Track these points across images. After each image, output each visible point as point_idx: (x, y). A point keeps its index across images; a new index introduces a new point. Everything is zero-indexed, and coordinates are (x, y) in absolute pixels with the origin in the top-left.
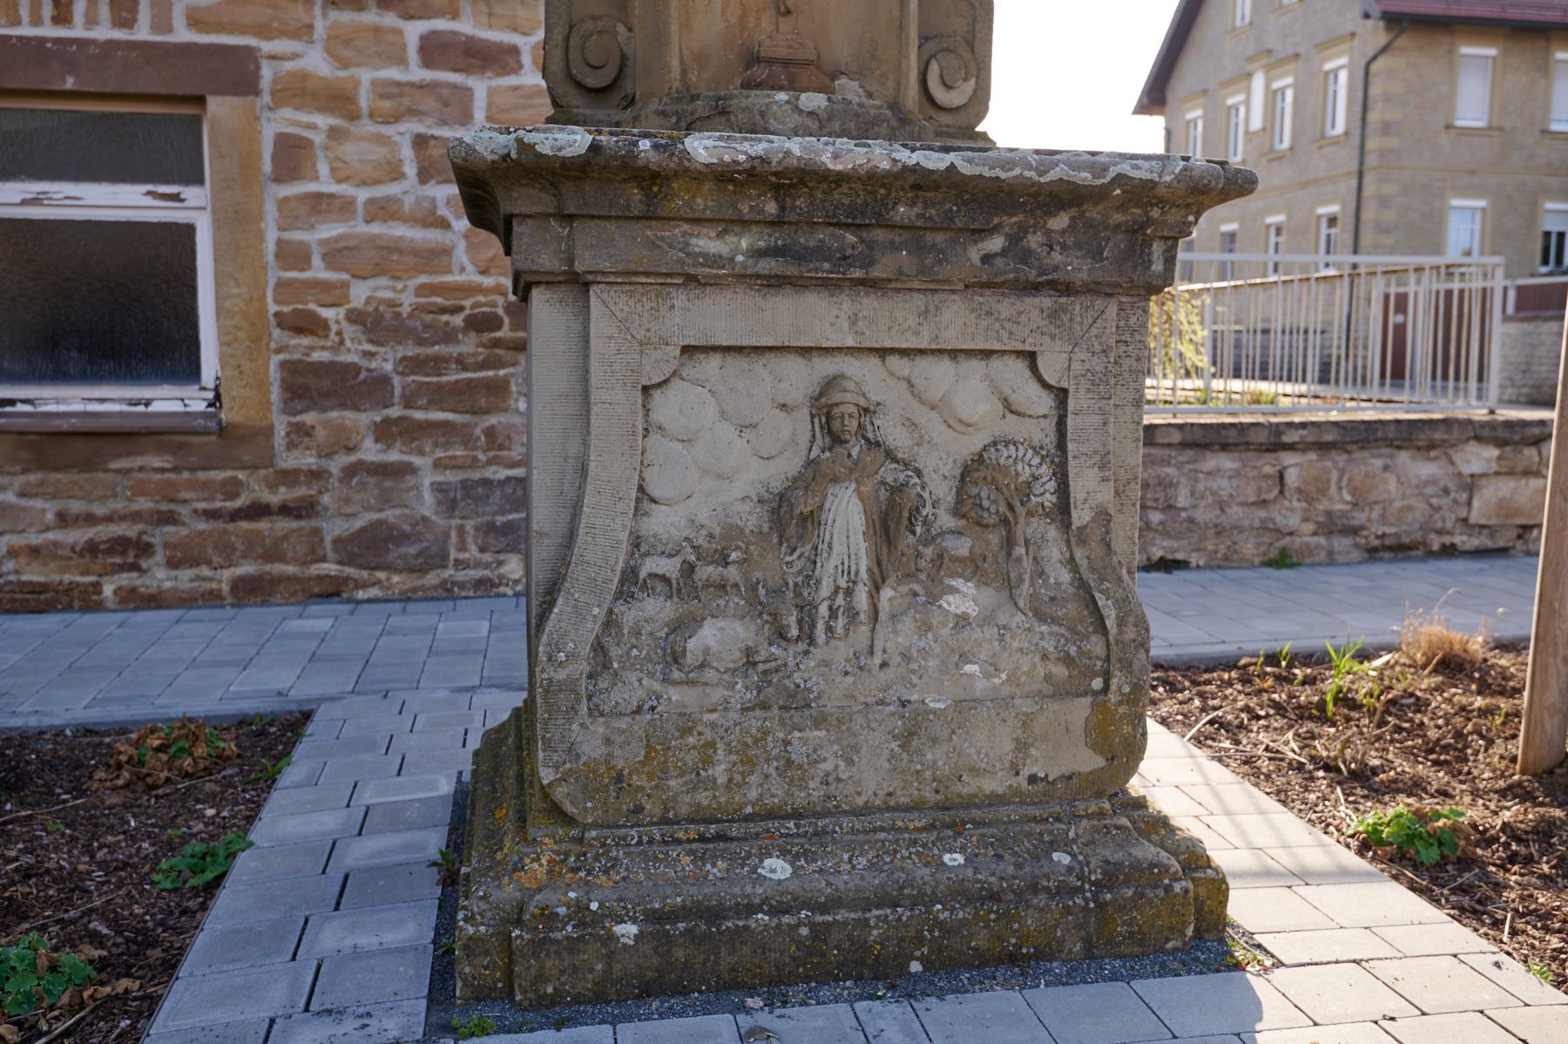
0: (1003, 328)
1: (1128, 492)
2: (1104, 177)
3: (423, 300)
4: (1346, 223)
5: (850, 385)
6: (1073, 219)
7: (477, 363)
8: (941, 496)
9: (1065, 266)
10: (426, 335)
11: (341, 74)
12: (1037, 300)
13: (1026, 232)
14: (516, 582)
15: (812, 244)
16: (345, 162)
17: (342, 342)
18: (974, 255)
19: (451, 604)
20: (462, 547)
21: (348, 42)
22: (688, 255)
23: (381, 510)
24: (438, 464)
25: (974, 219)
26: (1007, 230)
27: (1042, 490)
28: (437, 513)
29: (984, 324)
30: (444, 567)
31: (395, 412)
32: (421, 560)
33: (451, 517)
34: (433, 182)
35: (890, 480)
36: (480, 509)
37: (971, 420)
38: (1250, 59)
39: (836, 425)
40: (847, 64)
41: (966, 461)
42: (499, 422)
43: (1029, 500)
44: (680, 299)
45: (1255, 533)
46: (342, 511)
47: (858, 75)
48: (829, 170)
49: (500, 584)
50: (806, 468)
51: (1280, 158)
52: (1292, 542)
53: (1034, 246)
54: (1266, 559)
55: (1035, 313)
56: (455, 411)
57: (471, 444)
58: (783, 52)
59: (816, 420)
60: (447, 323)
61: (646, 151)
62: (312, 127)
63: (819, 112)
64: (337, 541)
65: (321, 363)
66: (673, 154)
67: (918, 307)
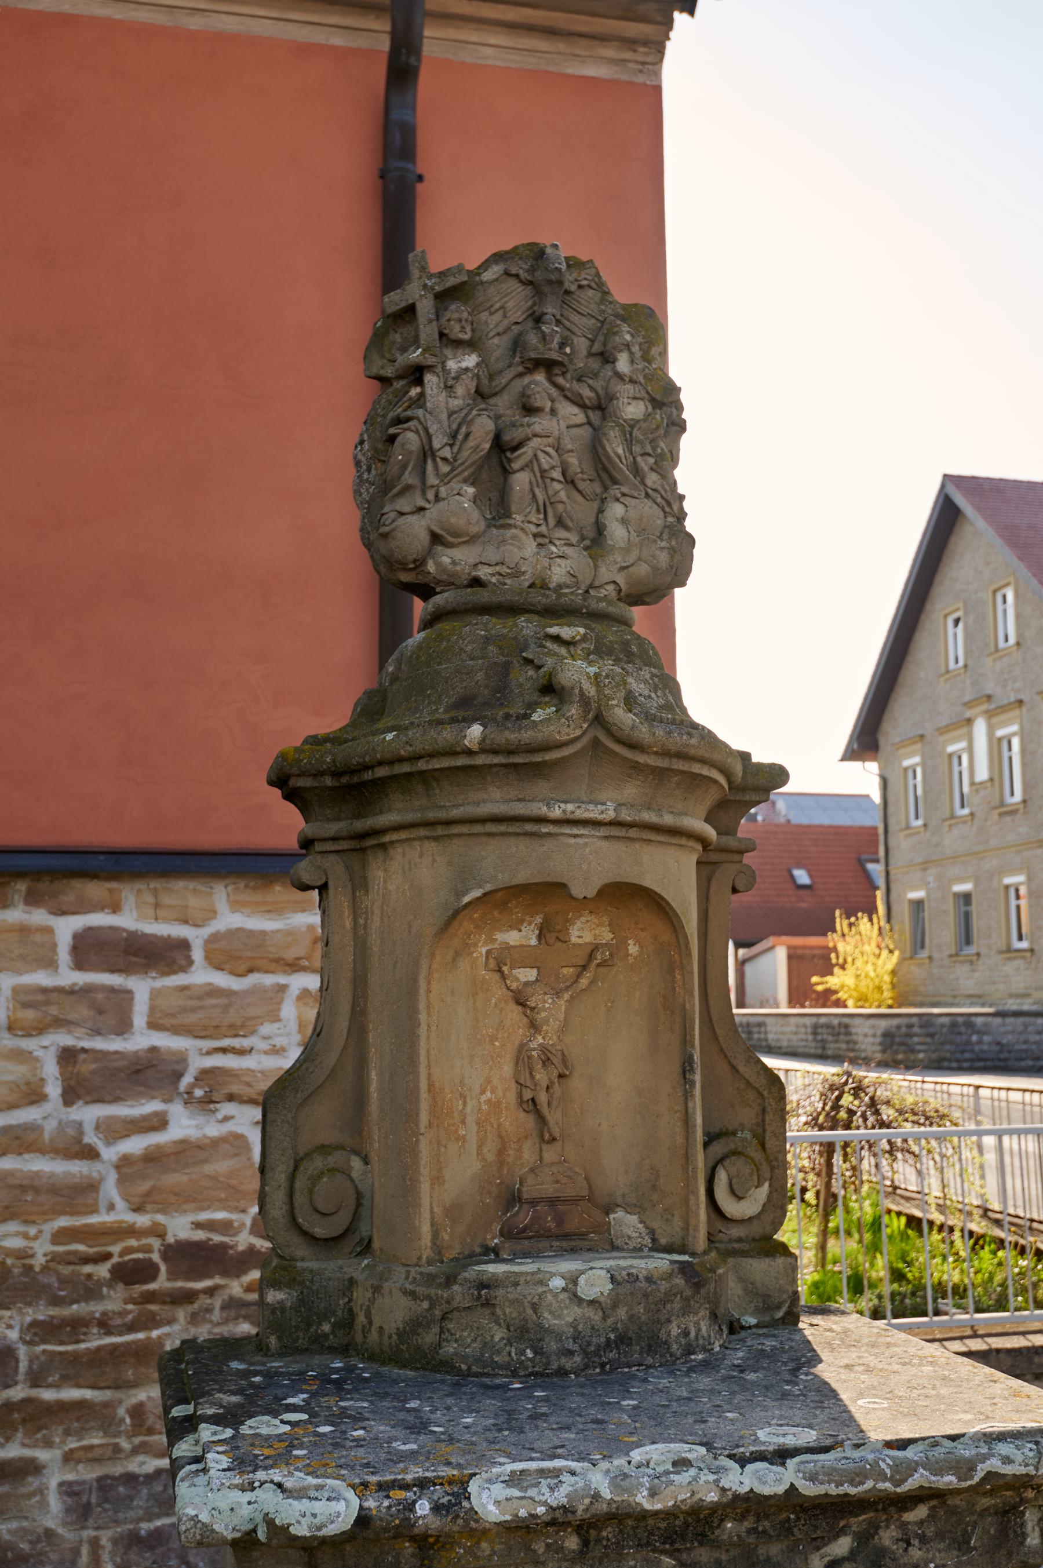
2: (972, 1478)
3: (60, 1249)
6: (932, 1509)
7: (124, 1325)
10: (62, 1293)
13: (877, 1528)
24: (68, 1458)
25: (816, 1527)
26: (854, 1528)
28: (64, 1524)
33: (83, 1528)
34: (80, 1103)
36: (121, 1515)
38: (968, 705)
40: (624, 1196)
42: (149, 1398)
47: (637, 1208)
48: (646, 1511)
51: (1013, 812)
53: (887, 1542)
56: (93, 1387)
57: (113, 1429)
58: (548, 1189)
60: (89, 1276)
61: (424, 1517)
63: (602, 1299)
66: (457, 1516)
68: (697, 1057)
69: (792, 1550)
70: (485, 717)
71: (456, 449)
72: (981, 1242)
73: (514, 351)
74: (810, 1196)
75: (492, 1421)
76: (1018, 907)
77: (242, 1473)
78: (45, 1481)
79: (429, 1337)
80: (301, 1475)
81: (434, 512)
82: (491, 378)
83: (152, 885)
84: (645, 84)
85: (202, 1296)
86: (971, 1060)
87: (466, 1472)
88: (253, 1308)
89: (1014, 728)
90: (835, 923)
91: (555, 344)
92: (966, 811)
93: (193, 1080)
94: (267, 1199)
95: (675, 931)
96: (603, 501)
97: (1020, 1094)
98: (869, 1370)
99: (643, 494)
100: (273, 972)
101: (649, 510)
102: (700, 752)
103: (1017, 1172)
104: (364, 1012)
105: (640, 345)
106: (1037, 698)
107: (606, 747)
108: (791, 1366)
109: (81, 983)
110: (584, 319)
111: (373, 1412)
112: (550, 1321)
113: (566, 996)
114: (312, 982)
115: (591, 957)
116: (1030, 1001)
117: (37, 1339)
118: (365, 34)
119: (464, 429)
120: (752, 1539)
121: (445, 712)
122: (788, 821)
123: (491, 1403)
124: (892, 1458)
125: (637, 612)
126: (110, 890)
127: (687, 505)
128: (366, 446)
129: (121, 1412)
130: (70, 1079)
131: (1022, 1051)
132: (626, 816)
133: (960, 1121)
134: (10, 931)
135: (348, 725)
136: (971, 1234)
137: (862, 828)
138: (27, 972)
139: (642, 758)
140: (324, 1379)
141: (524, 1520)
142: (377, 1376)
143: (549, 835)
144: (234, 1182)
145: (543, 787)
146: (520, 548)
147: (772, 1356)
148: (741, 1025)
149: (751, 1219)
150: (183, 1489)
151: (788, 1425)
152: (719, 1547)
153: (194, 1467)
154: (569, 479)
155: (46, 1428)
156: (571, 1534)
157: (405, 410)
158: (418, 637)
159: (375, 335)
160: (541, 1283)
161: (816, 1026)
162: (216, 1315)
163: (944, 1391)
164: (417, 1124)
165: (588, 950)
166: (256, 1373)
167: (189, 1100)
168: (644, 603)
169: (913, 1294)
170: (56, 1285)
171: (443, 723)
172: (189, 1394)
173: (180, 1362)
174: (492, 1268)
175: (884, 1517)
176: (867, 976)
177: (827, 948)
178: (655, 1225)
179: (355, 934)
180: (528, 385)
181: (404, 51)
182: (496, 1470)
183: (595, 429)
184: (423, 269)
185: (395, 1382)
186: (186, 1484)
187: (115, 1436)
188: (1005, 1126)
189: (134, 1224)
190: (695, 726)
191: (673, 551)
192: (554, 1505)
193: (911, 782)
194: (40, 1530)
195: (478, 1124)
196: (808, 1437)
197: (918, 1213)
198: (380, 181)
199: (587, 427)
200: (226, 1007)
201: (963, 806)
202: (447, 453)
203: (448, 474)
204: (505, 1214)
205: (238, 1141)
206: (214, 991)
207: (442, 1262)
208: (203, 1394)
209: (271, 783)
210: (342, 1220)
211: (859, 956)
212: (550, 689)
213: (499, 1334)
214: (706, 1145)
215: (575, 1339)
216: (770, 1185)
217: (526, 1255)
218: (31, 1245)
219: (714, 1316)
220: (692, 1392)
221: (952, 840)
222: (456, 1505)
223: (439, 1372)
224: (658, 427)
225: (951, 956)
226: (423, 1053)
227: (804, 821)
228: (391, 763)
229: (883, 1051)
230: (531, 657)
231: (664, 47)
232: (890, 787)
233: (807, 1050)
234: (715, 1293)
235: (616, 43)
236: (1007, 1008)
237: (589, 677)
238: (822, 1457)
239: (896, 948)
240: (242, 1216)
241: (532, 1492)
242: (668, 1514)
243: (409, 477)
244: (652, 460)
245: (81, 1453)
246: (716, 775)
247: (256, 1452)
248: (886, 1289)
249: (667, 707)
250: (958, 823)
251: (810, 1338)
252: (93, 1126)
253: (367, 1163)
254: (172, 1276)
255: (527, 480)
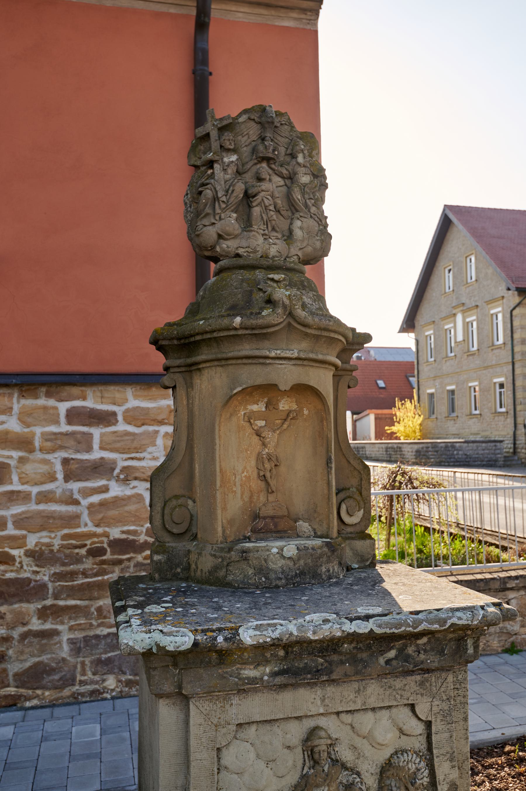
0: (397, 694)
1: (464, 767)
2: (445, 626)
4: (508, 386)
5: (322, 734)
6: (429, 638)
7: (93, 574)
8: (371, 785)
9: (427, 661)
10: (66, 561)
11: (26, 430)
12: (413, 677)
13: (407, 646)
14: (113, 690)
15: (301, 666)
16: (27, 474)
17: (22, 567)
18: (382, 661)
19: (76, 707)
20: (84, 673)
21: (29, 415)
22: (240, 679)
23: (40, 656)
24: (71, 629)
25: (381, 646)
26: (397, 647)
27: (422, 776)
28: (70, 656)
29: (388, 693)
30: (73, 685)
31: (49, 602)
32: (61, 682)
33: (78, 657)
34: (72, 481)
35: (344, 781)
36: (94, 652)
37: (384, 743)
38: (454, 307)
39: (316, 756)
40: (302, 515)
41: (382, 764)
42: (104, 604)
43: (415, 782)
44: (235, 700)
45: (497, 635)
46: (19, 658)
47: (308, 520)
48: (312, 640)
49: (104, 692)
50: (301, 780)
51: (473, 355)
52: (517, 638)
53: (410, 652)
54: (504, 648)
55: (413, 684)
57: (89, 617)
58: (271, 512)
59: (306, 753)
60: (77, 554)
61: (221, 643)
62: (11, 457)
63: (293, 557)
64: (16, 675)
65: (10, 579)
66: (234, 642)
67: (355, 688)
68: (333, 457)
69: (372, 655)
70: (242, 314)
71: (228, 197)
72: (456, 537)
73: (253, 153)
74: (383, 519)
75: (248, 606)
76: (475, 396)
77: (145, 626)
78: (61, 638)
79: (221, 573)
80: (170, 627)
81: (219, 225)
82: (243, 165)
83: (100, 388)
84: (310, 30)
85: (125, 561)
86: (454, 462)
87: (237, 625)
88: (147, 566)
89: (474, 318)
90: (395, 403)
91: (271, 150)
92: (453, 354)
93: (119, 471)
94: (153, 518)
95: (324, 404)
96: (292, 219)
97: (473, 474)
98: (404, 585)
99: (309, 216)
100: (152, 425)
101: (311, 223)
102: (334, 328)
103: (474, 509)
104: (192, 440)
105: (308, 150)
106: (484, 304)
107: (294, 326)
108: (372, 583)
109: (70, 430)
110: (283, 139)
111: (199, 603)
112: (271, 565)
113: (278, 432)
114: (170, 429)
115: (288, 415)
116: (479, 436)
117: (56, 580)
118: (185, 7)
119: (231, 188)
120: (355, 651)
121: (225, 311)
122: (376, 359)
123: (247, 599)
124: (413, 618)
125: (307, 268)
126: (82, 391)
127: (328, 221)
128: (189, 196)
129: (93, 609)
130: (67, 471)
131: (475, 458)
132: (302, 355)
133: (447, 486)
134: (39, 409)
135: (183, 318)
136: (451, 534)
137: (407, 362)
138: (47, 426)
139: (309, 331)
140: (178, 590)
141: (262, 643)
142: (200, 589)
143: (270, 364)
144: (137, 514)
145: (267, 344)
146: (256, 240)
147: (364, 580)
148: (355, 448)
149: (356, 524)
150: (121, 633)
151: (370, 606)
152: (341, 654)
153: (126, 625)
154: (277, 210)
155: (61, 616)
156: (281, 650)
157: (206, 180)
158: (213, 279)
159: (192, 146)
160: (268, 550)
161: (387, 448)
162: (132, 570)
163: (435, 592)
164: (215, 485)
165: (287, 412)
166: (150, 589)
167: (118, 479)
168: (310, 264)
169: (426, 558)
170: (64, 558)
171: (224, 317)
172: (122, 597)
173: (118, 585)
174: (247, 545)
175: (409, 642)
176: (409, 426)
177: (392, 414)
178: (316, 527)
179: (188, 407)
180: (259, 169)
181: (203, 15)
182: (250, 624)
183: (288, 188)
184: (213, 117)
185: (208, 591)
186: (123, 631)
187: (90, 620)
188: (467, 488)
189: (96, 532)
190: (332, 317)
191: (322, 241)
192: (274, 638)
193: (429, 342)
194: (60, 658)
195: (241, 485)
196: (379, 610)
197: (429, 526)
198: (193, 76)
199: (285, 187)
200: (133, 440)
201: (451, 352)
202: (224, 199)
203: (225, 208)
204: (253, 523)
205: (139, 497)
206: (127, 433)
207: (227, 543)
208: (129, 597)
209: (151, 343)
210: (185, 526)
211: (406, 418)
212: (270, 301)
213: (251, 572)
214: (337, 494)
215: (282, 573)
216: (364, 510)
217: (262, 539)
218: (52, 541)
219: (340, 564)
220: (331, 594)
221: (447, 367)
222: (234, 638)
223: (226, 587)
224: (316, 187)
225: (445, 417)
226: (217, 456)
227: (382, 359)
228: (202, 334)
229: (416, 459)
230: (261, 287)
231: (319, 12)
232: (420, 344)
233: (383, 458)
234: (341, 554)
235: (297, 11)
236: (469, 439)
237: (286, 296)
238: (384, 618)
239: (422, 414)
240: (141, 528)
241: (264, 633)
242: (320, 641)
243: (208, 210)
244: (313, 201)
245: (76, 627)
246: (341, 338)
247: (151, 618)
248: (415, 557)
249: (320, 309)
250: (449, 360)
251: (380, 573)
252: (77, 491)
253: (194, 503)
254: (113, 553)
255: (259, 210)
